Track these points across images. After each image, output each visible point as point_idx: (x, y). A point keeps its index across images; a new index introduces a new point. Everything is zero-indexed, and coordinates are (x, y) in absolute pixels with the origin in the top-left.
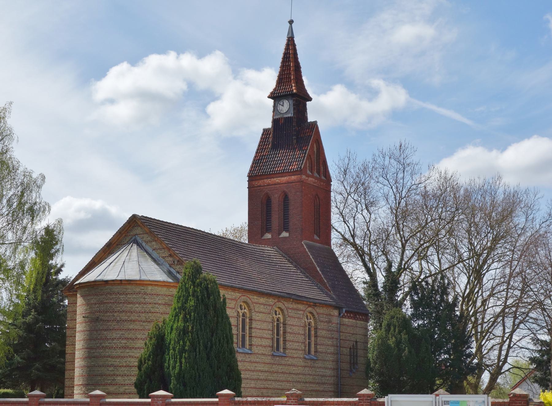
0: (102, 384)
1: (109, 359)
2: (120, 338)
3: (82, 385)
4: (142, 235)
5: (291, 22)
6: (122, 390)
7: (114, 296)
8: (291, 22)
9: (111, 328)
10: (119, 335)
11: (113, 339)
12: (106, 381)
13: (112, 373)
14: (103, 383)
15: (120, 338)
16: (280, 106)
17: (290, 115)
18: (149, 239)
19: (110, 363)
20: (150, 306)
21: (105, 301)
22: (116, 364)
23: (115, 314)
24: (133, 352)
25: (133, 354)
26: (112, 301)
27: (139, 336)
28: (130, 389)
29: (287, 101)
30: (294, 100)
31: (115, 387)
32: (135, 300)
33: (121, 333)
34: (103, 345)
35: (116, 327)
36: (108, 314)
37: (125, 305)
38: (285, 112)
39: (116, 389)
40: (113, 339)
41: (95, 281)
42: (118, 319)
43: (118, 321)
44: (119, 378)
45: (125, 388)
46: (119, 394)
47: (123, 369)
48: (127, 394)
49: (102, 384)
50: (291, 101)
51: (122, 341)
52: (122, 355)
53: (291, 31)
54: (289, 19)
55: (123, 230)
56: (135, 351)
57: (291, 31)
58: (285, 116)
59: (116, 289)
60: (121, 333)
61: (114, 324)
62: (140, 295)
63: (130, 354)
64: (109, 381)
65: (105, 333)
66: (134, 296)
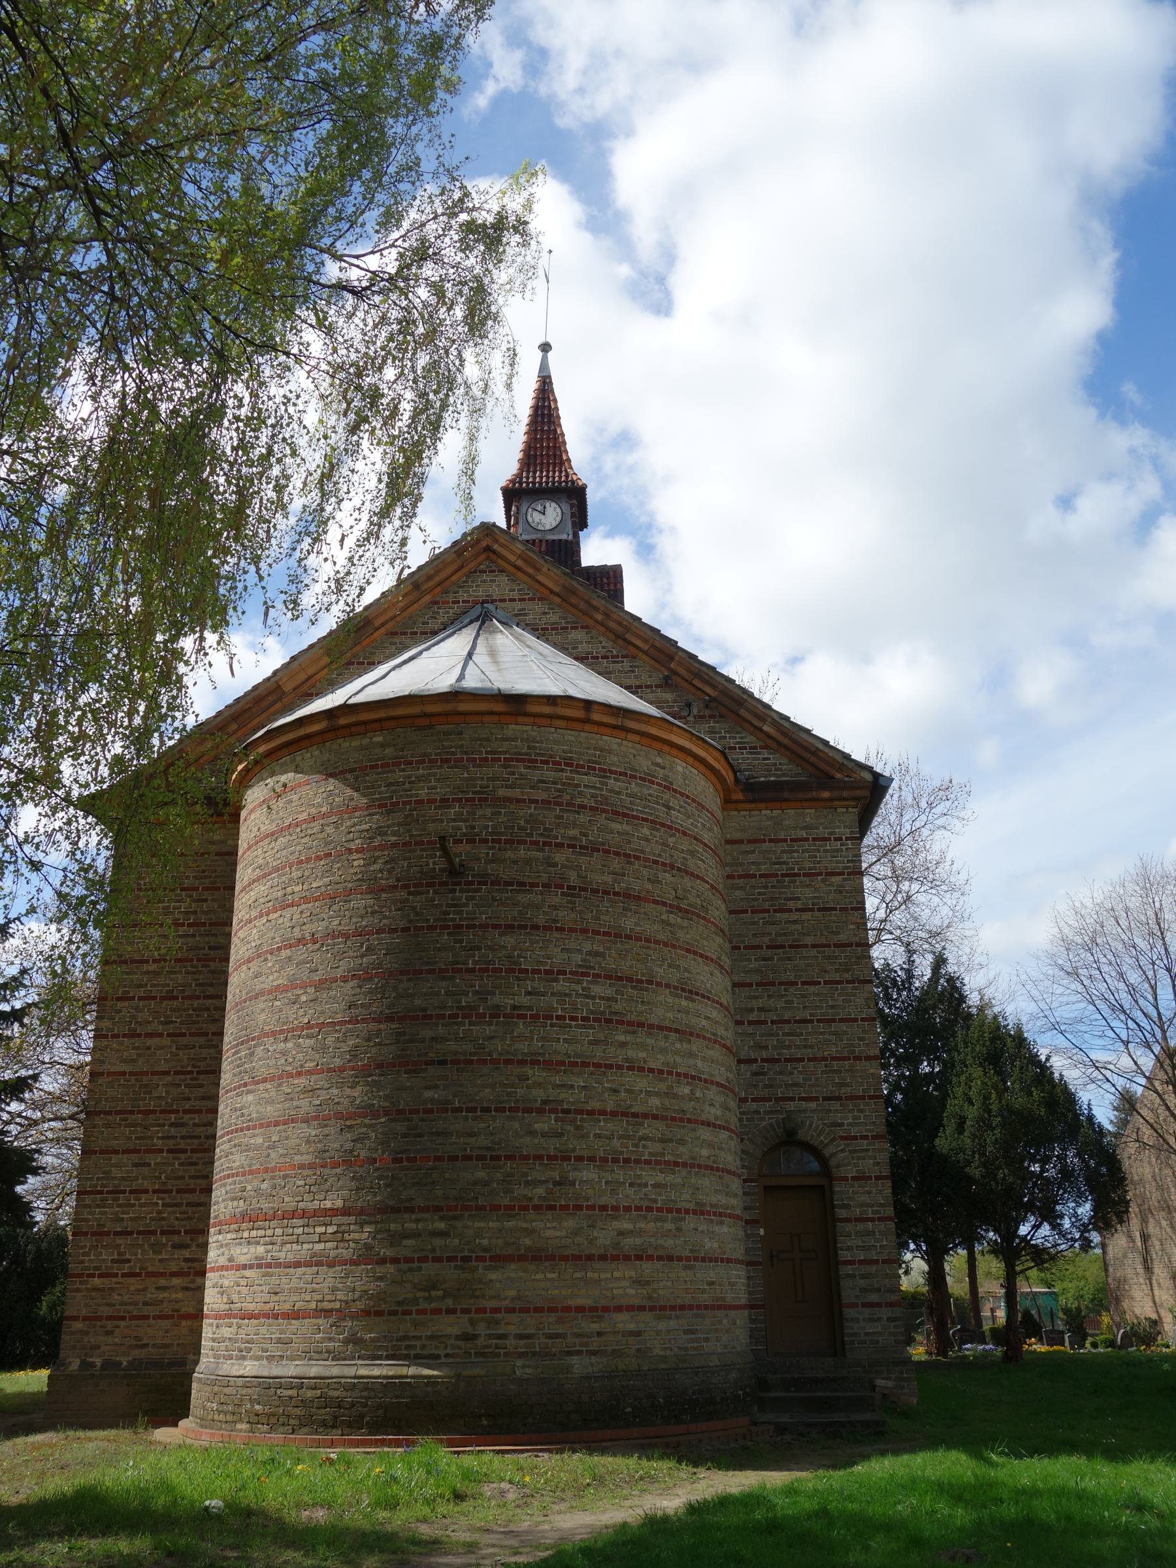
0: (496, 1208)
1: (536, 1074)
2: (581, 973)
3: (345, 1211)
4: (518, 605)
5: (545, 348)
6: (604, 1237)
7: (550, 775)
8: (545, 348)
9: (541, 920)
10: (577, 958)
11: (552, 975)
12: (521, 1191)
13: (552, 1146)
14: (506, 1202)
15: (581, 973)
16: (535, 514)
17: (564, 537)
18: (553, 618)
19: (539, 1094)
20: (685, 844)
21: (501, 792)
22: (570, 1098)
23: (560, 857)
24: (643, 1047)
25: (642, 1055)
26: (541, 795)
27: (660, 972)
28: (639, 1233)
29: (554, 505)
30: (572, 506)
31: (570, 1223)
32: (638, 808)
33: (587, 946)
34: (496, 999)
35: (566, 917)
36: (522, 853)
37: (602, 819)
38: (548, 527)
39: (576, 1232)
40: (552, 975)
41: (455, 695)
42: (573, 878)
43: (572, 892)
44: (588, 1174)
45: (616, 1225)
46: (590, 1258)
47: (605, 1126)
48: (627, 1258)
49: (496, 1208)
50: (566, 508)
51: (597, 990)
52: (598, 1054)
53: (544, 366)
54: (542, 340)
55: (430, 578)
56: (650, 1041)
57: (544, 366)
58: (551, 537)
59: (561, 740)
60: (587, 946)
61: (557, 900)
62: (654, 790)
63: (631, 1053)
64: (540, 1191)
65: (509, 940)
66: (634, 788)
